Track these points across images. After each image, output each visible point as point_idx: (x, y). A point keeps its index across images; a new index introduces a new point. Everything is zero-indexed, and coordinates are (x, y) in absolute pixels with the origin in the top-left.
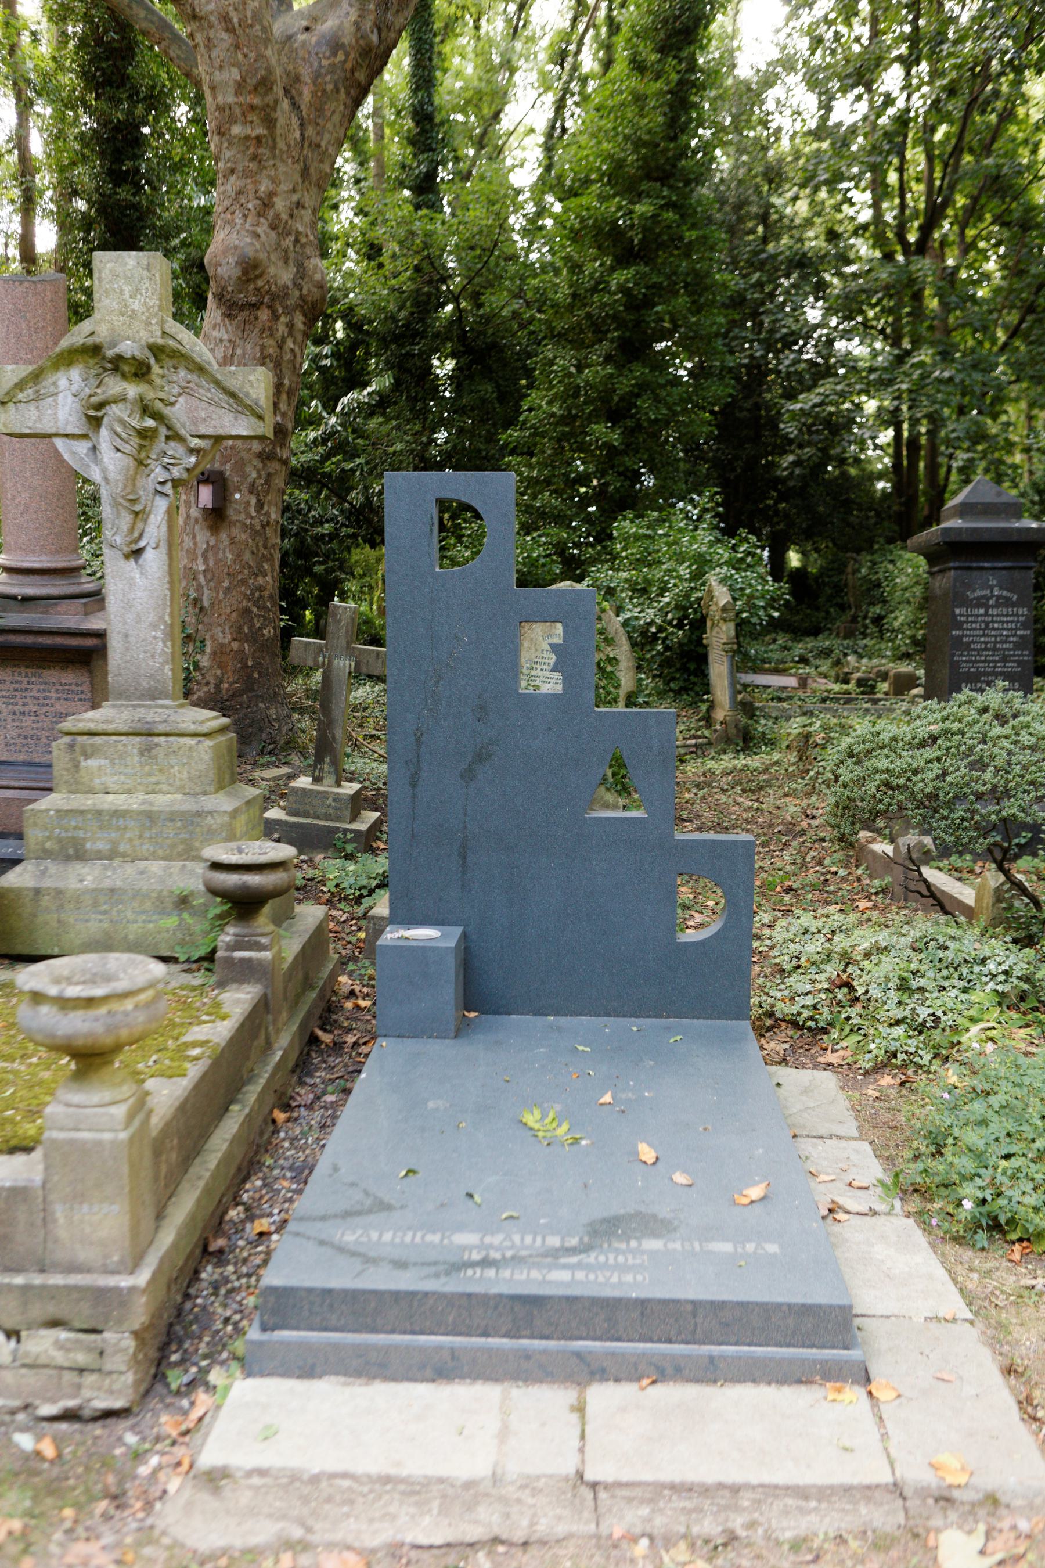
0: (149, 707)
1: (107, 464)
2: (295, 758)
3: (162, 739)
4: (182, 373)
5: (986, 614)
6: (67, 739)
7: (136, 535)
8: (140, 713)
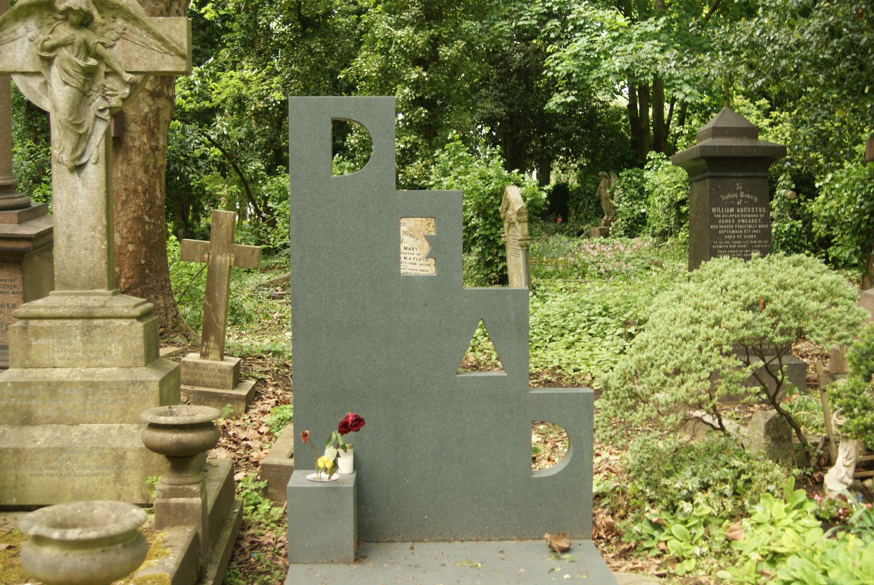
0: (89, 294)
1: (55, 96)
2: (178, 339)
3: (101, 322)
4: (120, 22)
5: (735, 212)
6: (19, 323)
7: (79, 152)
8: (82, 300)
